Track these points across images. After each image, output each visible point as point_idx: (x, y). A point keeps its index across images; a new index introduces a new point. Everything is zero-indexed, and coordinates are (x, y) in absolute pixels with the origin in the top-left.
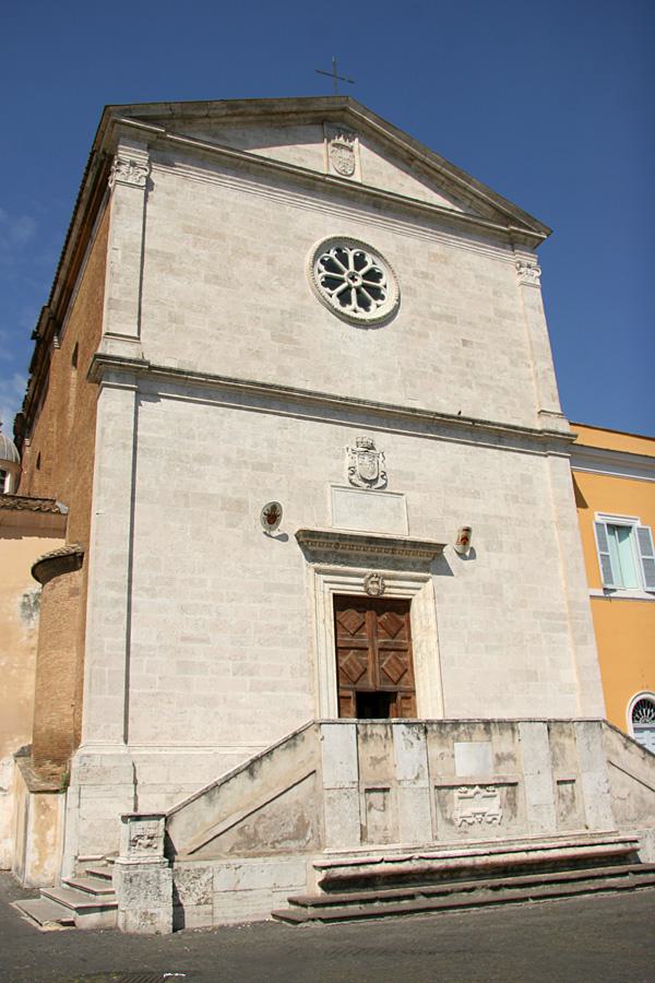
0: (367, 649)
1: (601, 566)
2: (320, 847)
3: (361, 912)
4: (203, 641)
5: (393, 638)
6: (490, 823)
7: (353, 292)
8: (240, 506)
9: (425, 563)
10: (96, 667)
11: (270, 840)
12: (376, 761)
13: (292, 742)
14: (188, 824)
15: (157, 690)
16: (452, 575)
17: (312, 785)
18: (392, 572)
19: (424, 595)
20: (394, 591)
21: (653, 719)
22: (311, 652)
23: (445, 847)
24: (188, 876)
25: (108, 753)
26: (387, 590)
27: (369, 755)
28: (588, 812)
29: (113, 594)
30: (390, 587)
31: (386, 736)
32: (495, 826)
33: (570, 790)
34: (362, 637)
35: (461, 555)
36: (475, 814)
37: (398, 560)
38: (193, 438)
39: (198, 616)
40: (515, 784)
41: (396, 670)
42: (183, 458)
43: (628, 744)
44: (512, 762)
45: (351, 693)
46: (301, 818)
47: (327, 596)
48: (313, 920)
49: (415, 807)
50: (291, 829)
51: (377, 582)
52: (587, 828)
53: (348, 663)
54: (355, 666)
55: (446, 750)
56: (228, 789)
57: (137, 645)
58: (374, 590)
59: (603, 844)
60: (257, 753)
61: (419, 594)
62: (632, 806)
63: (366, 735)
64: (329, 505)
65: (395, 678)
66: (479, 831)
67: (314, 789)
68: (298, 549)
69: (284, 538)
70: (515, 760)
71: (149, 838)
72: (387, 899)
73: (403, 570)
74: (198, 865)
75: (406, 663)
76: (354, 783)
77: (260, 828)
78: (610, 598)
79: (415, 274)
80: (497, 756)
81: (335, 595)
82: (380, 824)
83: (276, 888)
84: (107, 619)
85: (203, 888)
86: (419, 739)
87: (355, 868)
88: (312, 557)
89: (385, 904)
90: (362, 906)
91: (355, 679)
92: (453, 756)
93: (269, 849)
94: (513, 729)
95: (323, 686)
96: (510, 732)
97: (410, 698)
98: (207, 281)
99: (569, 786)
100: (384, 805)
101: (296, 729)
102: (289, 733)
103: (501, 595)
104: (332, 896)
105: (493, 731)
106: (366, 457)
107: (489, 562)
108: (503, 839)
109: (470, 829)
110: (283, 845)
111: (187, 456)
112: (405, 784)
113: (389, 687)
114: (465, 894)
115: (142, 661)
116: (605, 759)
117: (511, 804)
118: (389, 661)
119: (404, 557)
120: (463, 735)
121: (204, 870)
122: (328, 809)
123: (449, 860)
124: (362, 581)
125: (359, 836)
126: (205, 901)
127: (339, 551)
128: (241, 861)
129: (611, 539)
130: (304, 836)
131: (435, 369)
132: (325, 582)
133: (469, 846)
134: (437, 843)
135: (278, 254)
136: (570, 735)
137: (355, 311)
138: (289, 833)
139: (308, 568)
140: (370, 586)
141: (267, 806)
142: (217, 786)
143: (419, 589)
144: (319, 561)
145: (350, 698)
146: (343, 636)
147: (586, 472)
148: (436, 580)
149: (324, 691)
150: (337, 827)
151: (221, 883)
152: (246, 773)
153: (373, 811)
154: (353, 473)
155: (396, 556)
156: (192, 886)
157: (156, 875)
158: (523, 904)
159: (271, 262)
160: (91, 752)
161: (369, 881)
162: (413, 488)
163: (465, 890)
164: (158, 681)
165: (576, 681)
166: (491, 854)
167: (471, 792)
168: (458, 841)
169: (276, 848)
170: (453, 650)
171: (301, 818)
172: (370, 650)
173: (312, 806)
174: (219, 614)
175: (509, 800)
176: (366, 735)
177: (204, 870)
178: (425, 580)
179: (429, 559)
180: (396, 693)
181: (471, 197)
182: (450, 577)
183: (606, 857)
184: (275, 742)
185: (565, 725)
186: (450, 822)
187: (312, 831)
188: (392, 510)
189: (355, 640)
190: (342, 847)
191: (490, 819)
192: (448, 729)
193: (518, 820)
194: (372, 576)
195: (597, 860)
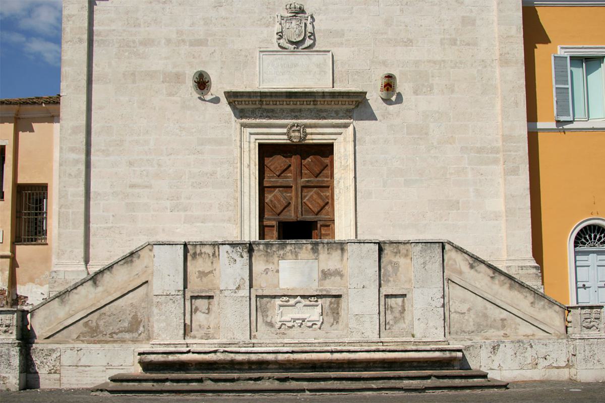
1: (555, 99)
2: (149, 338)
3: (154, 389)
5: (316, 177)
8: (178, 78)
9: (349, 111)
10: (63, 210)
11: (109, 332)
12: (202, 274)
13: (129, 259)
14: (45, 318)
15: (110, 225)
16: (374, 118)
17: (145, 292)
18: (265, 121)
19: (345, 139)
20: (317, 135)
21: (603, 243)
22: (236, 191)
23: (261, 345)
24: (42, 353)
25: (70, 270)
26: (309, 137)
28: (416, 323)
29: (73, 156)
30: (312, 134)
31: (214, 254)
32: (315, 330)
34: (286, 177)
35: (387, 101)
36: (295, 320)
37: (321, 111)
38: (139, 25)
39: (143, 168)
40: (339, 296)
42: (132, 44)
43: (475, 264)
44: (338, 278)
45: (274, 223)
46: (135, 317)
47: (252, 145)
48: (102, 390)
49: (295, 309)
50: (126, 325)
51: (299, 131)
53: (273, 199)
54: (279, 201)
55: (270, 266)
56: (77, 294)
57: (95, 192)
58: (296, 137)
59: (349, 352)
61: (340, 138)
62: (471, 320)
63: (195, 254)
64: (258, 69)
65: (316, 210)
67: (147, 295)
68: (228, 109)
69: (216, 100)
70: (342, 276)
71: (6, 326)
72: (178, 381)
73: (325, 118)
75: (327, 197)
76: (179, 291)
77: (101, 323)
78: (564, 131)
81: (260, 145)
83: (109, 366)
84: (70, 175)
87: (165, 355)
88: (240, 113)
89: (175, 384)
90: (155, 384)
91: (279, 211)
93: (108, 338)
95: (246, 217)
96: (339, 252)
97: (328, 226)
99: (399, 300)
100: (208, 309)
102: (127, 251)
103: (426, 134)
104: (148, 375)
106: (294, 22)
107: (414, 104)
109: (290, 332)
110: (120, 335)
111: (134, 42)
112: (226, 293)
113: (310, 217)
114: (252, 382)
115: (99, 204)
117: (335, 313)
118: (312, 196)
119: (327, 107)
121: (54, 350)
122: (155, 310)
124: (285, 130)
126: (54, 371)
127: (264, 107)
129: (579, 72)
130: (137, 330)
132: (251, 134)
133: (284, 345)
134: (253, 341)
138: (124, 327)
139: (235, 123)
140: (293, 134)
141: (107, 307)
142: (67, 292)
143: (340, 134)
144: (246, 117)
145: (273, 226)
146: (270, 177)
147: (554, 6)
148: (362, 125)
150: (163, 325)
151: (66, 359)
153: (198, 313)
154: (281, 37)
155: (319, 107)
156: (45, 361)
157: (7, 352)
158: (299, 394)
160: (58, 269)
161: (183, 366)
162: (342, 44)
164: (111, 218)
165: (502, 208)
166: (293, 352)
167: (292, 301)
169: (113, 338)
170: (367, 188)
171: (135, 317)
172: (293, 187)
173: (144, 308)
174: (159, 165)
176: (195, 254)
177: (54, 350)
178: (346, 126)
179: (352, 107)
180: (316, 222)
182: (374, 122)
183: (427, 362)
184: (115, 259)
185: (401, 247)
186: (271, 325)
187: (144, 326)
188: (318, 66)
189: (280, 180)
190: (166, 338)
191: (310, 324)
192: (274, 249)
193: (341, 326)
194: (294, 126)
195: (415, 364)
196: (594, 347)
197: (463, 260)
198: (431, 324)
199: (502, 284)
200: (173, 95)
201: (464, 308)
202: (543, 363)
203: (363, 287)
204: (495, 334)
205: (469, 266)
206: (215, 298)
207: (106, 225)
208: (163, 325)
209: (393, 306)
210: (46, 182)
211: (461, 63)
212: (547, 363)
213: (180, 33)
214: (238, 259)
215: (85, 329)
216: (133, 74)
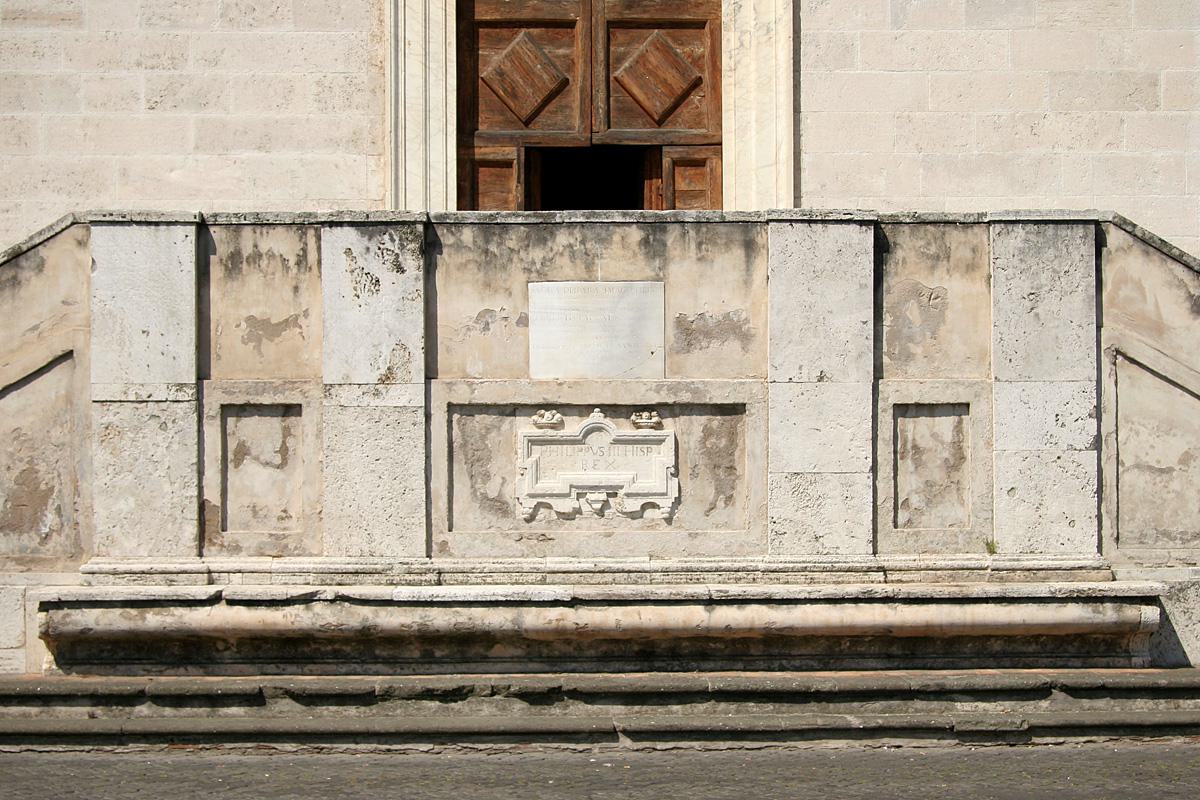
0: (571, 24)
2: (76, 552)
3: (96, 727)
6: (633, 515)
12: (262, 330)
23: (464, 575)
27: (245, 313)
28: (1001, 502)
33: (948, 437)
36: (581, 491)
41: (665, 82)
44: (733, 345)
45: (511, 152)
46: (28, 477)
52: (991, 549)
53: (507, 67)
54: (528, 73)
55: (498, 303)
59: (768, 601)
65: (657, 106)
66: (801, 526)
67: (69, 400)
72: (178, 700)
75: (697, 61)
76: (181, 386)
80: (681, 323)
82: (271, 501)
86: (400, 269)
87: (133, 612)
89: (168, 711)
90: (99, 711)
92: (523, 321)
94: (750, 246)
96: (738, 253)
97: (701, 163)
99: (945, 424)
100: (284, 451)
101: (19, 238)
104: (75, 680)
108: (673, 563)
112: (345, 396)
113: (635, 133)
116: (754, 346)
117: (723, 466)
118: (642, 59)
120: (565, 260)
122: (99, 455)
123: (434, 612)
125: (192, 529)
130: (35, 522)
136: (971, 267)
145: (508, 164)
149: (414, 147)
150: (126, 505)
153: (248, 465)
158: (596, 747)
161: (195, 649)
163: (429, 694)
166: (575, 602)
167: (574, 426)
168: (509, 563)
171: (28, 477)
172: (579, 25)
173: (60, 446)
185: (955, 236)
186: (500, 506)
187: (59, 510)
191: (634, 505)
193: (740, 512)
197: (1170, 285)
203: (821, 379)
205: (1188, 305)
206: (304, 412)
209: (922, 443)
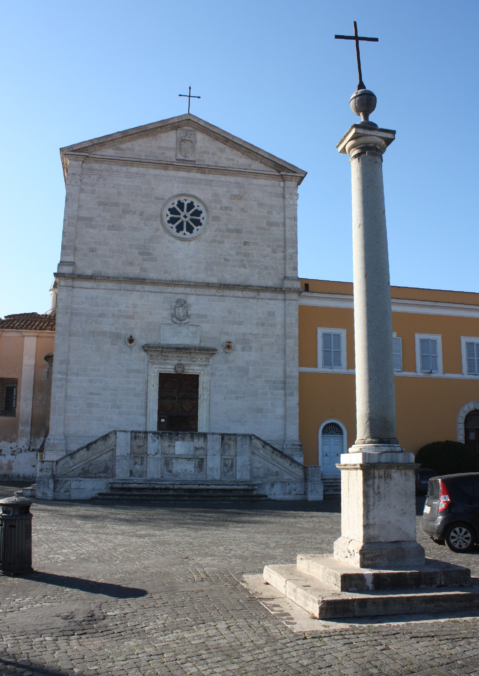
4: (98, 394)
7: (185, 224)
20: (192, 369)
28: (237, 472)
31: (145, 437)
46: (106, 466)
60: (91, 441)
67: (112, 455)
74: (65, 479)
77: (90, 468)
79: (221, 208)
81: (160, 373)
84: (58, 386)
85: (67, 487)
86: (158, 439)
96: (203, 438)
98: (109, 229)
105: (195, 438)
111: (95, 315)
112: (150, 456)
122: (117, 463)
128: (82, 479)
131: (226, 260)
135: (145, 209)
137: (185, 234)
150: (120, 470)
152: (85, 449)
153: (137, 465)
159: (141, 214)
171: (106, 466)
175: (199, 465)
181: (261, 157)
188: (193, 333)
196: (315, 485)
198: (244, 473)
199: (277, 455)
200: (115, 345)
201: (260, 465)
202: (294, 493)
204: (273, 478)
207: (76, 415)
208: (120, 470)
210: (16, 377)
211: (267, 335)
212: (295, 492)
213: (119, 311)
214: (157, 440)
215: (82, 472)
216: (93, 332)
